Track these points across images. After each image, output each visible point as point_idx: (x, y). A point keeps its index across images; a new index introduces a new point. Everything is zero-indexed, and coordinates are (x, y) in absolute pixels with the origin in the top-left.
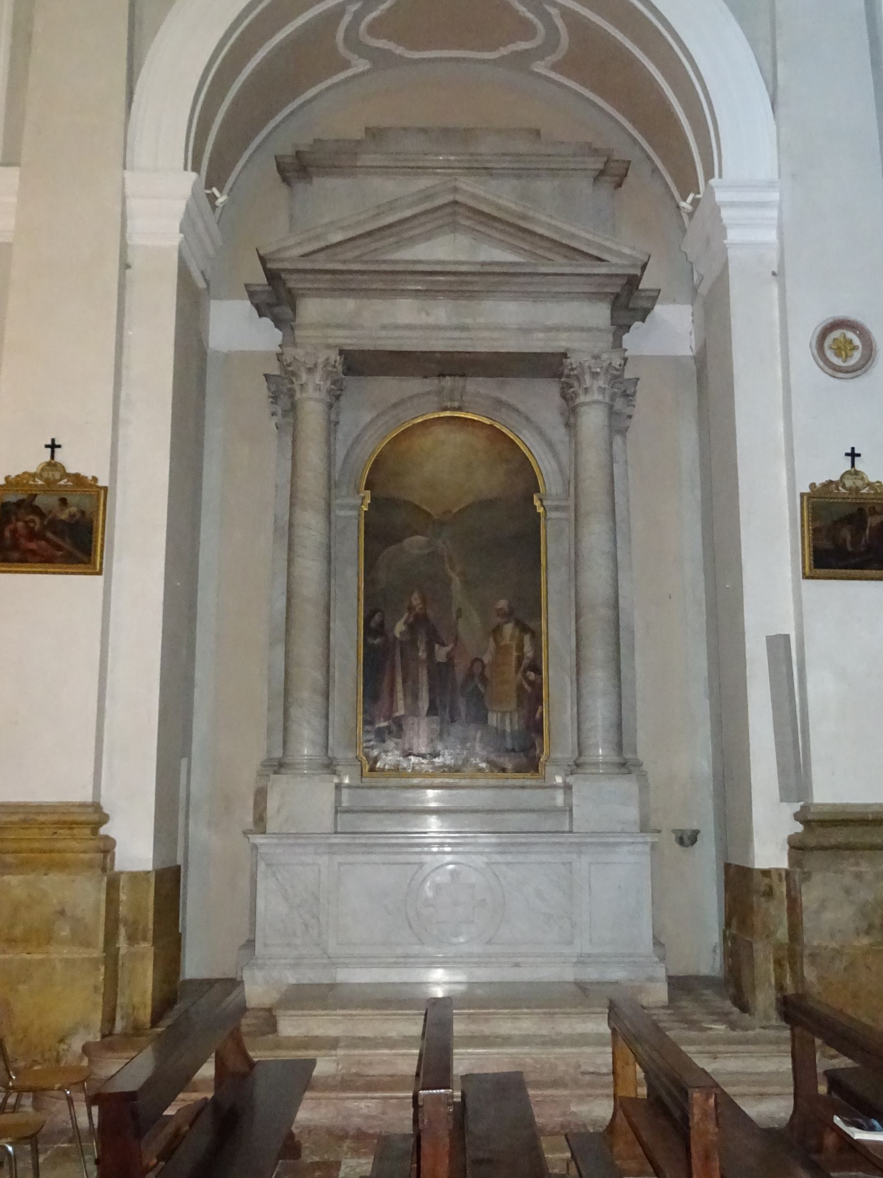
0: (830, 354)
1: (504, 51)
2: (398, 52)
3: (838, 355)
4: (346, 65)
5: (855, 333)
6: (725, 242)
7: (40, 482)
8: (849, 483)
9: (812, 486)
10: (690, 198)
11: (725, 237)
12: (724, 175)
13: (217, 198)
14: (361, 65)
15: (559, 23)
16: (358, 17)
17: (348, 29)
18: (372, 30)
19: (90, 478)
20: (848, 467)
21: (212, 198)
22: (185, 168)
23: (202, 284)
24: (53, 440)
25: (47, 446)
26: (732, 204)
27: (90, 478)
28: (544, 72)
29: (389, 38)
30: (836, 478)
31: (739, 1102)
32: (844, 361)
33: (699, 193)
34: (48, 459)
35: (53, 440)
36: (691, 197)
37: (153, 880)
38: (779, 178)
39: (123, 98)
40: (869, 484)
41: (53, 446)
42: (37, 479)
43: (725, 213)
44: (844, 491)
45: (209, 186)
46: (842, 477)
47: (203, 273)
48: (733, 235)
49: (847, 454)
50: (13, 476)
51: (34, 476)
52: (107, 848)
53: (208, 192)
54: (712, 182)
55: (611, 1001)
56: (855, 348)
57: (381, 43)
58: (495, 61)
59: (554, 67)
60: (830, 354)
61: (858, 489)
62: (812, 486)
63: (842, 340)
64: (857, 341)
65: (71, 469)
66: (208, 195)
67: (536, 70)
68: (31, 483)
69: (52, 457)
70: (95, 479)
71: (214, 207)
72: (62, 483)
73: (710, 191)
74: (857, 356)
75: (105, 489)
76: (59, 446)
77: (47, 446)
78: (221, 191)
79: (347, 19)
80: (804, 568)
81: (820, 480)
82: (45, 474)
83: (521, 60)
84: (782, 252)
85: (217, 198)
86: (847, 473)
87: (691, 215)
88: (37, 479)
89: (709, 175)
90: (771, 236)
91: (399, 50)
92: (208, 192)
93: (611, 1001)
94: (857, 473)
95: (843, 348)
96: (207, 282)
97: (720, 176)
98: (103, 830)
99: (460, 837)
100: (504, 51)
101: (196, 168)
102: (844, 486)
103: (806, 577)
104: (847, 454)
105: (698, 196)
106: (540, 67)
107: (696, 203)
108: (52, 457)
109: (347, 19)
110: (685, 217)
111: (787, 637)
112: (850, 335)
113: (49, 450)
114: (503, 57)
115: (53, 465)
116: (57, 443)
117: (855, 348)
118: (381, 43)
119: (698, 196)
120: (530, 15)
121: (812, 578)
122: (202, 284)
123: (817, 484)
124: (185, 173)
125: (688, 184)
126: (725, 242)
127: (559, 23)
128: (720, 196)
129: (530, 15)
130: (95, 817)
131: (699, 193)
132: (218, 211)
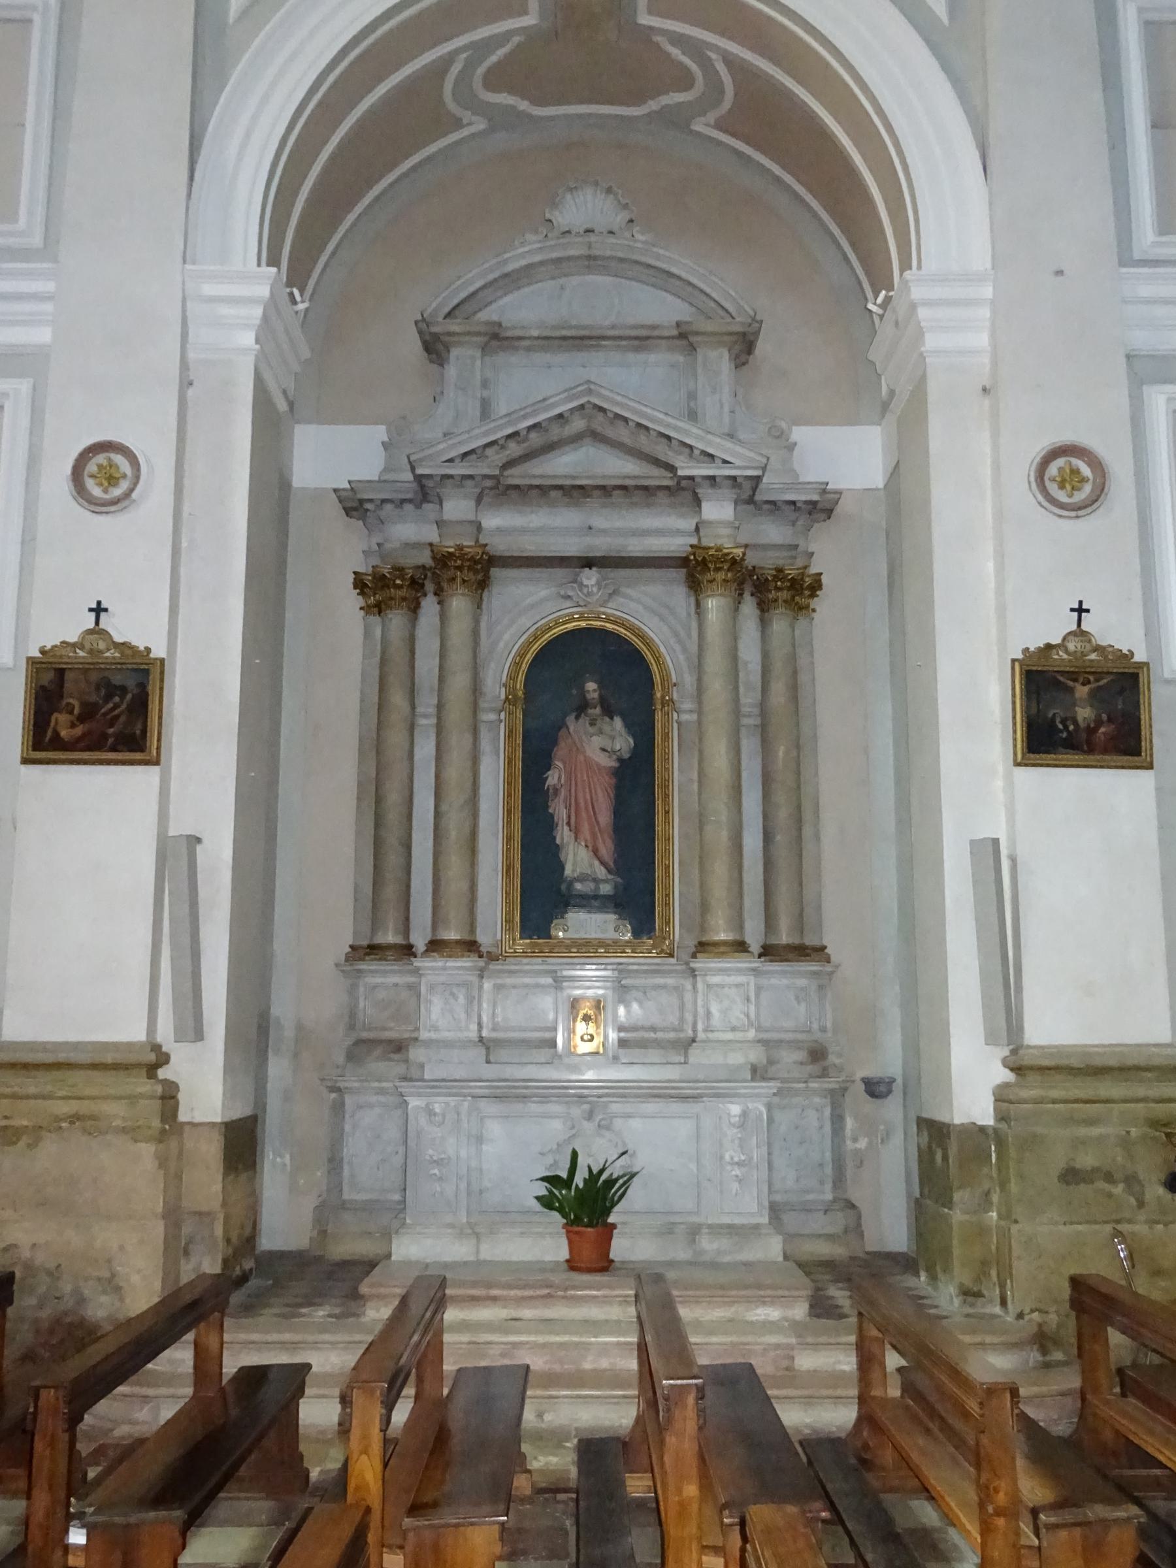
0: (1053, 488)
2: (522, 108)
3: (1062, 486)
4: (458, 124)
6: (923, 349)
7: (81, 653)
8: (1071, 646)
10: (879, 300)
11: (923, 344)
14: (480, 125)
16: (470, 66)
17: (457, 83)
20: (91, 625)
22: (259, 265)
23: (282, 406)
24: (99, 603)
25: (91, 610)
26: (929, 303)
27: (142, 648)
29: (512, 91)
30: (73, 638)
31: (773, 1400)
32: (1070, 496)
33: (893, 290)
34: (91, 625)
35: (99, 603)
38: (993, 269)
41: (99, 610)
42: (78, 651)
43: (923, 313)
44: (1065, 656)
45: (290, 284)
46: (1064, 639)
47: (285, 392)
48: (931, 342)
50: (49, 647)
51: (74, 646)
52: (169, 1096)
54: (907, 274)
59: (719, 126)
60: (1053, 488)
61: (1084, 655)
64: (1086, 471)
65: (118, 638)
68: (71, 654)
69: (97, 622)
70: (148, 650)
72: (108, 654)
73: (905, 283)
74: (97, 492)
75: (162, 661)
76: (1088, 611)
77: (91, 610)
80: (1015, 754)
81: (51, 641)
82: (1071, 646)
83: (676, 120)
84: (995, 364)
86: (1070, 633)
87: (881, 317)
88: (78, 651)
89: (906, 265)
90: (982, 340)
91: (524, 105)
94: (104, 633)
95: (1068, 478)
96: (291, 405)
97: (919, 267)
98: (162, 1073)
99: (505, 1087)
100: (653, 105)
101: (273, 261)
102: (1067, 651)
103: (26, 761)
105: (891, 294)
108: (97, 622)
110: (876, 319)
111: (996, 842)
113: (93, 615)
115: (97, 631)
116: (104, 605)
117: (1084, 480)
119: (891, 294)
121: (1026, 765)
122: (282, 406)
123: (1032, 649)
124: (259, 269)
125: (881, 279)
128: (917, 293)
130: (152, 1057)
131: (893, 290)
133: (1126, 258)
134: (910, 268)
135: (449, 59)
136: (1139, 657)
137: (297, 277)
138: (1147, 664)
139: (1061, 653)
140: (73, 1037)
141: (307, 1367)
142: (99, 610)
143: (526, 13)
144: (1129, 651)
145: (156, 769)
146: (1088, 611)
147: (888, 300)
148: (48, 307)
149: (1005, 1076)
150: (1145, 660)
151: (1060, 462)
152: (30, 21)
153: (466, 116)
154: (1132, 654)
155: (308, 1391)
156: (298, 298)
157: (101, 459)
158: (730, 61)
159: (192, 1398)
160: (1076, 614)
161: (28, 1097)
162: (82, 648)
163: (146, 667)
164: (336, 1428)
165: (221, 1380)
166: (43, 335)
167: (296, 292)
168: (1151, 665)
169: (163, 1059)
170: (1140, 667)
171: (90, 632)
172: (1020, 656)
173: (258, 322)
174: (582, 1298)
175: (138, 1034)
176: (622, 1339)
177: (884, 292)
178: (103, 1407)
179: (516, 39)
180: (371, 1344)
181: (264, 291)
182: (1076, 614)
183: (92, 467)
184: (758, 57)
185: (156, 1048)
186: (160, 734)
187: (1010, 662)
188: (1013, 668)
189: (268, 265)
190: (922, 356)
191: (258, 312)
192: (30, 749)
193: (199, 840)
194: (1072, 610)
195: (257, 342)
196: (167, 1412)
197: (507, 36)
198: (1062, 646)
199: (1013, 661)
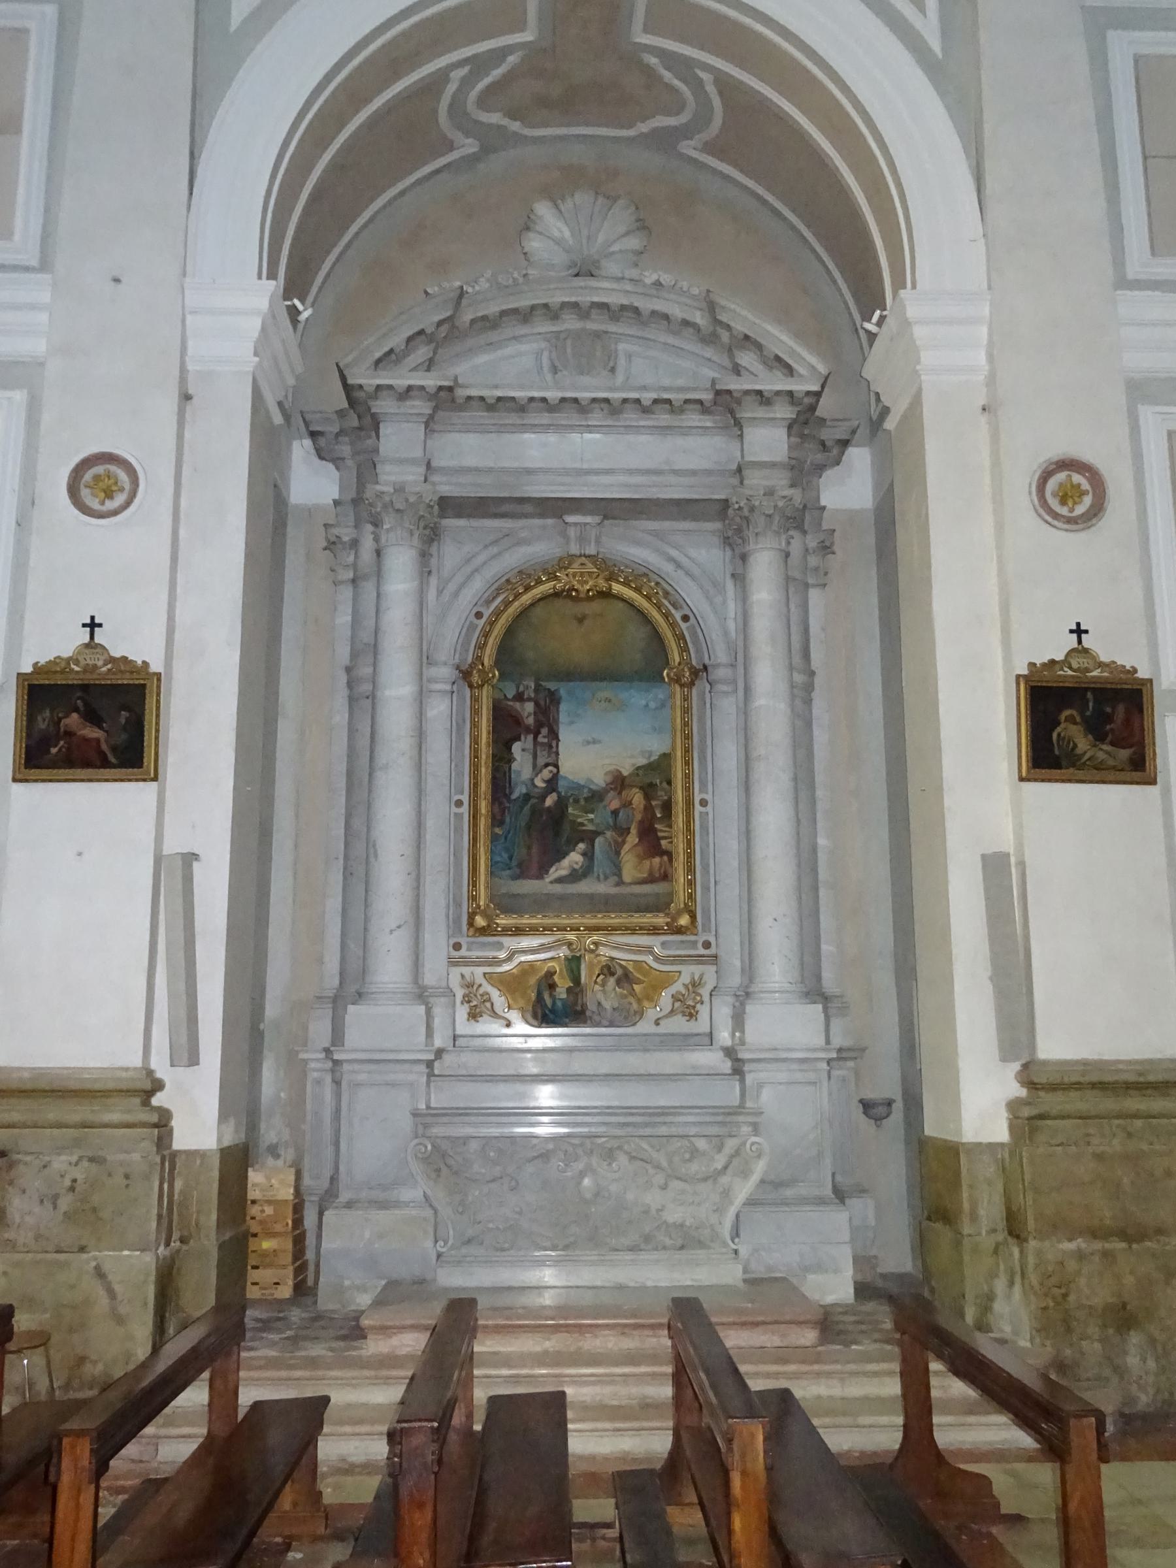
1: (644, 128)
2: (518, 123)
4: (451, 147)
5: (1084, 476)
9: (1032, 665)
11: (918, 362)
12: (918, 287)
13: (299, 313)
15: (711, 89)
16: (466, 83)
18: (484, 102)
19: (139, 662)
21: (293, 313)
22: (260, 277)
24: (93, 618)
27: (139, 662)
28: (695, 154)
30: (1060, 656)
34: (87, 639)
35: (93, 618)
36: (878, 313)
37: (216, 1162)
39: (186, 192)
40: (1101, 665)
41: (93, 625)
44: (1070, 673)
45: (287, 295)
47: (280, 404)
48: (928, 358)
49: (1071, 631)
51: (68, 660)
52: (162, 1123)
53: (289, 303)
54: (902, 293)
55: (863, 1050)
56: (1085, 493)
57: (495, 118)
58: (630, 140)
59: (709, 148)
61: (1088, 670)
62: (1032, 665)
63: (1069, 485)
64: (1085, 485)
65: (116, 653)
66: (287, 306)
67: (685, 151)
69: (1080, 642)
70: (146, 664)
71: (294, 322)
76: (100, 625)
78: (303, 302)
79: (452, 88)
81: (45, 657)
83: (665, 140)
85: (299, 313)
86: (1073, 650)
87: (872, 337)
89: (899, 283)
92: (289, 303)
93: (863, 1050)
94: (1086, 651)
97: (914, 287)
98: (156, 1101)
100: (644, 128)
101: (272, 276)
102: (1070, 668)
103: (15, 780)
104: (1071, 631)
105: (885, 313)
106: (689, 148)
107: (880, 324)
108: (1080, 642)
109: (452, 88)
112: (1077, 478)
113: (1075, 636)
114: (642, 135)
115: (91, 645)
116: (97, 621)
118: (495, 118)
119: (885, 313)
120: (676, 83)
121: (1029, 780)
122: (278, 419)
124: (260, 282)
126: (918, 367)
127: (711, 89)
129: (676, 83)
130: (148, 1086)
131: (885, 309)
132: (300, 327)
133: (1123, 283)
134: (904, 287)
135: (442, 77)
136: (1142, 674)
137: (295, 287)
138: (1151, 681)
139: (1066, 669)
140: (40, 1063)
141: (326, 1400)
142: (93, 625)
143: (522, 30)
144: (1132, 667)
145: (154, 784)
146: (100, 625)
147: (882, 319)
148: (43, 317)
149: (1018, 1091)
150: (1147, 677)
151: (1061, 476)
152: (25, 31)
153: (458, 137)
154: (1135, 671)
155: (326, 1429)
156: (300, 307)
157: (99, 469)
158: (725, 84)
159: (206, 1438)
160: (88, 629)
161: (106, 1126)
162: (77, 663)
163: (142, 682)
164: (385, 1461)
165: (237, 1417)
166: (37, 346)
167: (296, 302)
168: (1154, 683)
169: (158, 1086)
170: (1143, 685)
171: (87, 646)
172: (1026, 672)
173: (256, 334)
174: (520, 1326)
175: (137, 1062)
176: (551, 1371)
177: (878, 311)
178: (131, 1450)
179: (512, 59)
180: (412, 1378)
181: (264, 304)
182: (88, 629)
183: (88, 476)
184: (420, 70)
185: (150, 1073)
186: (157, 754)
187: (1014, 678)
188: (1018, 684)
189: (268, 278)
190: (916, 373)
191: (256, 324)
192: (23, 767)
193: (195, 856)
194: (84, 625)
195: (256, 354)
196: (187, 1449)
197: (500, 55)
198: (1066, 662)
199: (1018, 677)
